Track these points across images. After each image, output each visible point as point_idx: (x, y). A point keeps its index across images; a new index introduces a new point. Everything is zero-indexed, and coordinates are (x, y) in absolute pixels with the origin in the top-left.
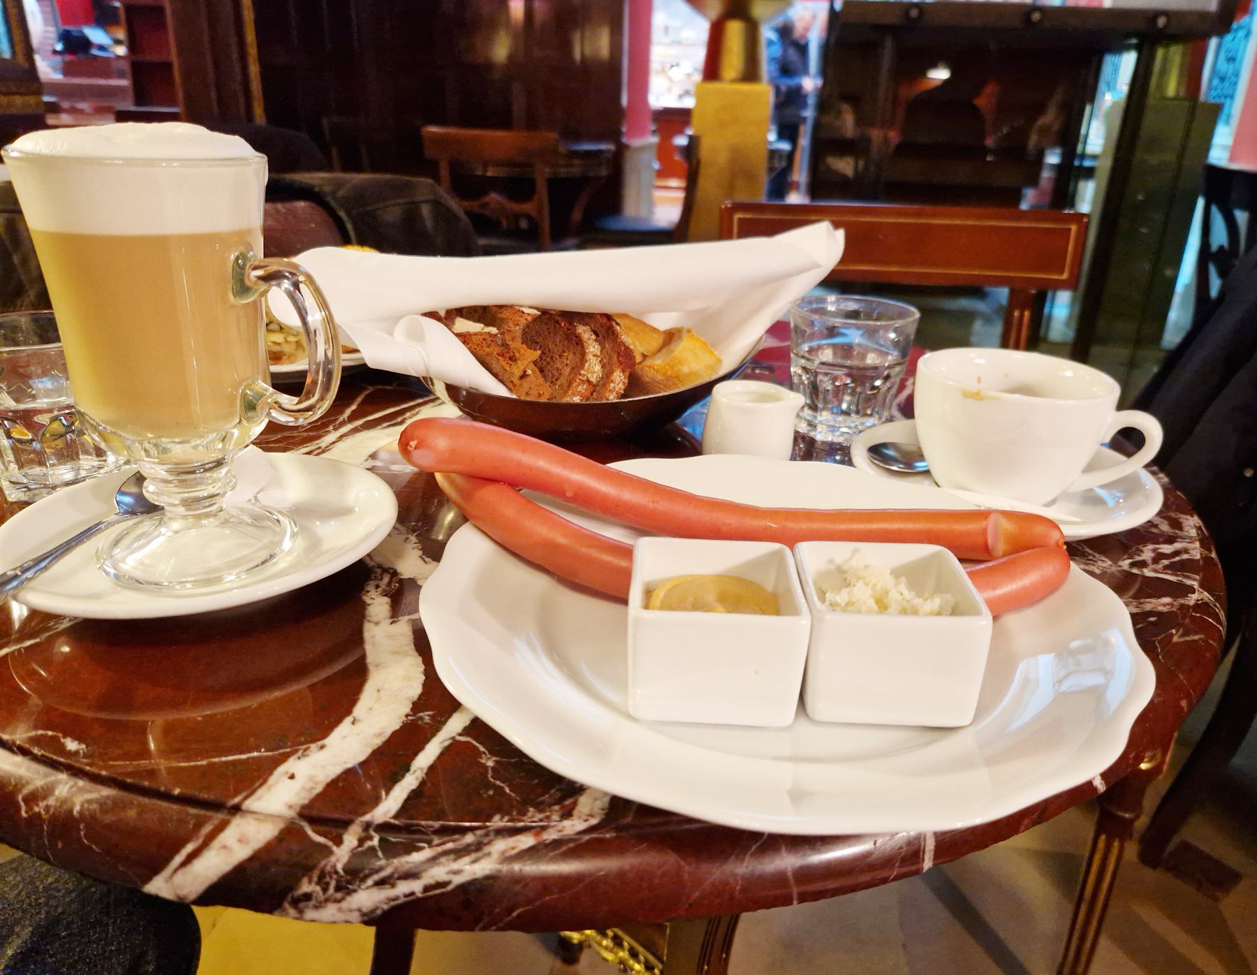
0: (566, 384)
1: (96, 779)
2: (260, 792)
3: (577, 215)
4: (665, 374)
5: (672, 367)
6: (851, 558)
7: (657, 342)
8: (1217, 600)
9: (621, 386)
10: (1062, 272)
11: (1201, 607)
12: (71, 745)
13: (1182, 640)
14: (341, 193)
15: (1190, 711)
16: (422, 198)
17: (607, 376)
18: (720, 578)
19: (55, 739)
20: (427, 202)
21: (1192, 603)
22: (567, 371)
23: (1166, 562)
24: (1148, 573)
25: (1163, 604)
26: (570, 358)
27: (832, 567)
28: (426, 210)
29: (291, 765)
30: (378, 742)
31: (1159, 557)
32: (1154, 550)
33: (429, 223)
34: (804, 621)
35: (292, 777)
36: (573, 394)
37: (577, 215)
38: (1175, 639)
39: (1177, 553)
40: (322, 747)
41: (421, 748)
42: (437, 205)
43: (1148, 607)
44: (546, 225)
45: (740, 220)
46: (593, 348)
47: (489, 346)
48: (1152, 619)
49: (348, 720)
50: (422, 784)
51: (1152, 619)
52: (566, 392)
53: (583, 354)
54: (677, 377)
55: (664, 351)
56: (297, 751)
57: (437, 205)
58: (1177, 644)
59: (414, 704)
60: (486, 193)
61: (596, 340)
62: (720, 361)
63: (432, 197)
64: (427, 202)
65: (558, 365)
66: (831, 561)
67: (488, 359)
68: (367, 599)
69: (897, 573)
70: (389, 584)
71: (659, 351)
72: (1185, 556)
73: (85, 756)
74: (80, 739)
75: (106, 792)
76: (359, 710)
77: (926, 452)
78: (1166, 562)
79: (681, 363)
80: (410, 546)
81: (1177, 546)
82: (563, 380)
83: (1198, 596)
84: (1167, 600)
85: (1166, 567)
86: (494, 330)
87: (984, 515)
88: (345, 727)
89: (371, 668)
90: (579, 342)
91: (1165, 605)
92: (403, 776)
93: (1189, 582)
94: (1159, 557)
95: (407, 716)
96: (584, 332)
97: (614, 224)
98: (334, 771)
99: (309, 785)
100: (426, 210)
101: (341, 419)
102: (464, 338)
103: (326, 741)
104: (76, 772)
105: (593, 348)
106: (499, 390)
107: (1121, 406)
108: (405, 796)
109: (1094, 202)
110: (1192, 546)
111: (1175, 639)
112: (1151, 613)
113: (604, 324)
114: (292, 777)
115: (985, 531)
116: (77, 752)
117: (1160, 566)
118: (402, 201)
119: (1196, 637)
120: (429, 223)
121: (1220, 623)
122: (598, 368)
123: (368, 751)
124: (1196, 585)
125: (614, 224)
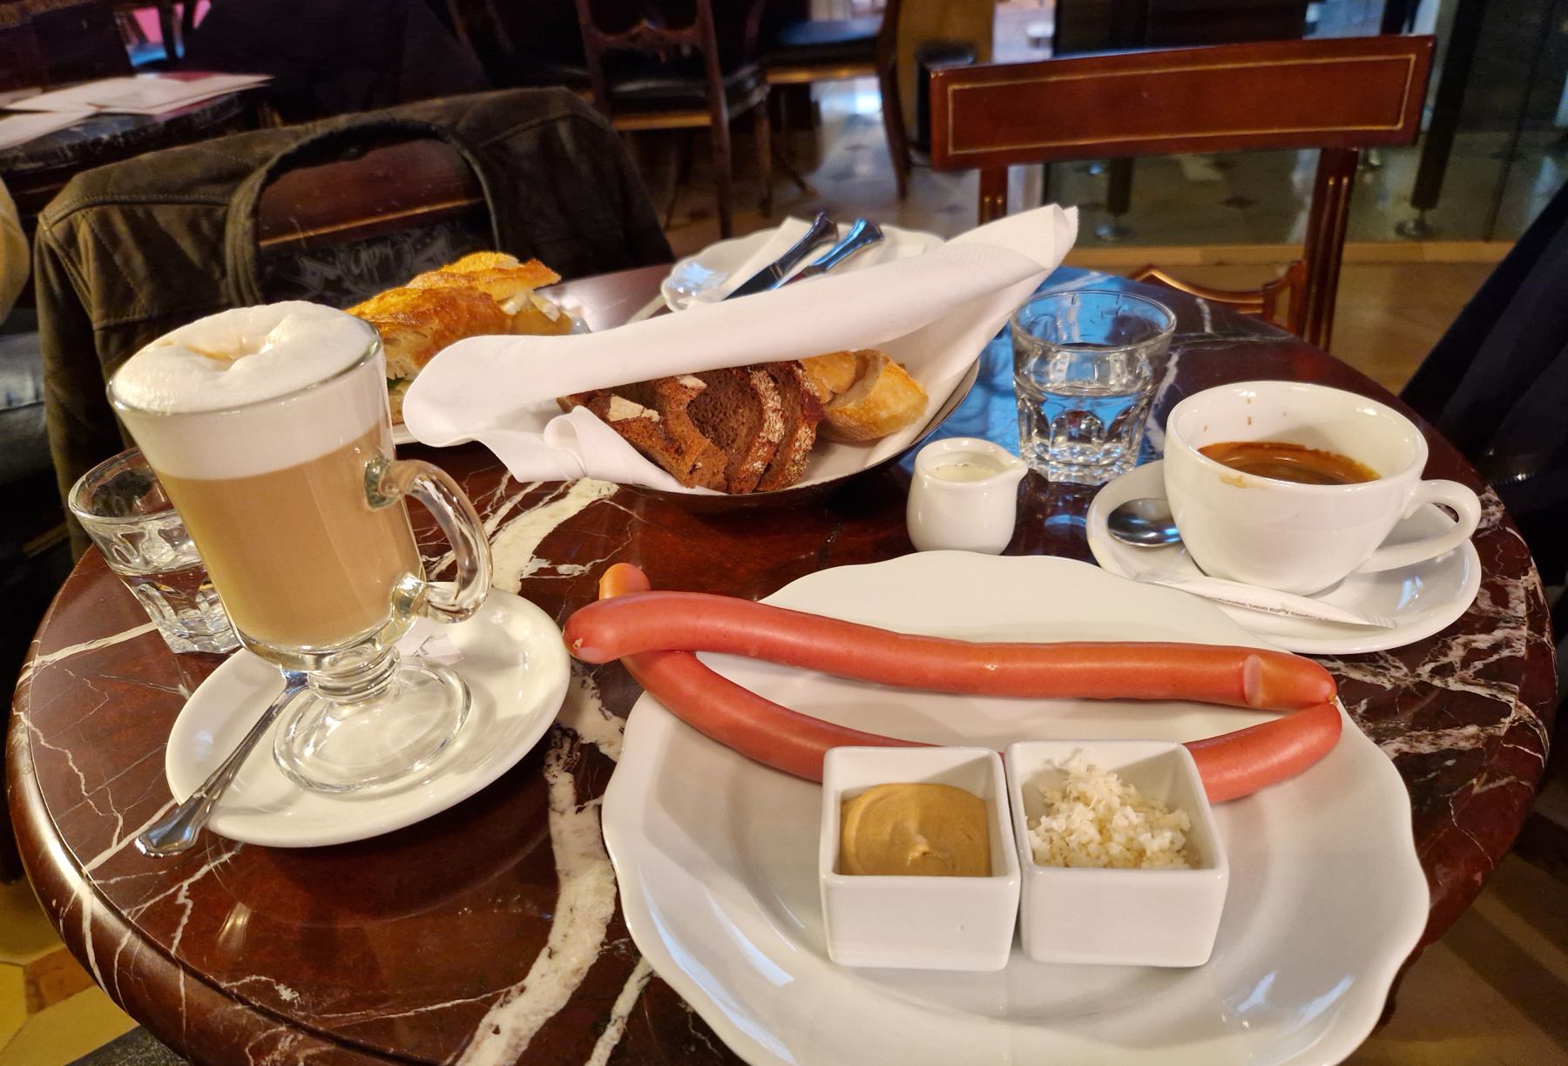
0: (743, 448)
1: (313, 1033)
2: (468, 1051)
3: (752, 27)
4: (860, 419)
5: (868, 412)
6: (1073, 756)
7: (846, 373)
8: (1538, 716)
9: (809, 442)
10: (1396, 123)
11: (1520, 732)
12: (286, 994)
13: (1485, 788)
14: (462, 124)
15: (1484, 884)
16: (559, 114)
17: (790, 434)
18: (923, 786)
19: (268, 985)
20: (563, 118)
21: (1503, 732)
22: (744, 431)
23: (1479, 665)
24: (1454, 685)
25: (1465, 736)
26: (745, 414)
27: (1049, 767)
28: (563, 131)
29: (496, 1016)
30: (577, 981)
31: (1473, 654)
32: (1465, 645)
33: (569, 147)
34: (1012, 883)
35: (497, 1031)
36: (754, 461)
37: (752, 27)
38: (1476, 790)
39: (1496, 647)
40: (523, 990)
41: (620, 990)
42: (578, 122)
43: (1446, 743)
44: (714, 58)
45: (955, 92)
46: (772, 402)
47: (650, 437)
48: (1450, 763)
49: (545, 951)
50: (624, 1037)
51: (1450, 763)
52: (745, 459)
53: (761, 412)
54: (875, 423)
55: (857, 387)
56: (498, 996)
57: (578, 122)
58: (1477, 795)
59: (608, 927)
60: (635, 21)
61: (775, 388)
62: (925, 399)
63: (568, 112)
64: (563, 118)
65: (733, 423)
66: (1049, 762)
67: (651, 451)
68: (551, 780)
69: (1128, 775)
70: (570, 752)
71: (852, 385)
72: (1506, 653)
73: (302, 1008)
74: (292, 986)
75: (325, 1047)
76: (555, 938)
77: (1178, 519)
78: (1479, 665)
79: (877, 407)
80: (588, 693)
81: (1499, 634)
82: (740, 442)
83: (1520, 711)
84: (1472, 729)
85: (1478, 674)
86: (654, 415)
87: (1239, 653)
88: (541, 964)
89: (562, 877)
90: (755, 396)
91: (1468, 738)
92: (605, 1028)
93: (1505, 698)
94: (1473, 654)
95: (602, 944)
96: (762, 383)
97: (802, 37)
98: (538, 1022)
99: (514, 1041)
100: (563, 131)
101: (498, 494)
102: (621, 427)
103: (526, 982)
104: (295, 1026)
105: (772, 402)
106: (668, 484)
107: (1428, 474)
108: (607, 1054)
109: (1440, 23)
110: (1517, 633)
111: (1476, 790)
112: (1448, 754)
113: (785, 373)
114: (497, 1031)
115: (1240, 674)
116: (291, 1004)
117: (1471, 672)
118: (534, 122)
119: (1503, 782)
120: (569, 147)
121: (1540, 749)
122: (779, 425)
123: (568, 994)
124: (1512, 699)
125: (802, 37)
